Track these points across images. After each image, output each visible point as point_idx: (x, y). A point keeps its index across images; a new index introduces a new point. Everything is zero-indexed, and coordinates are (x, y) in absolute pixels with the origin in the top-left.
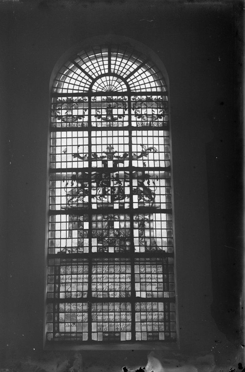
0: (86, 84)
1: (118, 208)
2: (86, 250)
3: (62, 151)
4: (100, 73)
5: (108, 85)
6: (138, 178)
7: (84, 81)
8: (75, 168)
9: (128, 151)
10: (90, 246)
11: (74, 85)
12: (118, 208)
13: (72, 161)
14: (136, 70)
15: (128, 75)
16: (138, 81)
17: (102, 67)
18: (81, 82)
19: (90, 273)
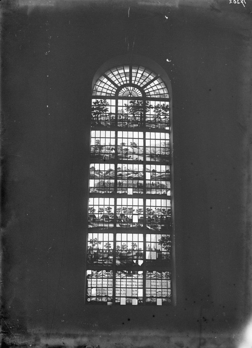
0: (112, 91)
1: (137, 304)
2: (117, 213)
3: (124, 104)
4: (136, 83)
5: (126, 91)
6: (160, 122)
7: (110, 88)
8: (113, 131)
9: (142, 296)
10: (118, 223)
11: (108, 89)
12: (137, 304)
13: (100, 138)
14: (152, 81)
15: (144, 84)
16: (152, 87)
17: (141, 81)
18: (108, 89)
19: (114, 279)
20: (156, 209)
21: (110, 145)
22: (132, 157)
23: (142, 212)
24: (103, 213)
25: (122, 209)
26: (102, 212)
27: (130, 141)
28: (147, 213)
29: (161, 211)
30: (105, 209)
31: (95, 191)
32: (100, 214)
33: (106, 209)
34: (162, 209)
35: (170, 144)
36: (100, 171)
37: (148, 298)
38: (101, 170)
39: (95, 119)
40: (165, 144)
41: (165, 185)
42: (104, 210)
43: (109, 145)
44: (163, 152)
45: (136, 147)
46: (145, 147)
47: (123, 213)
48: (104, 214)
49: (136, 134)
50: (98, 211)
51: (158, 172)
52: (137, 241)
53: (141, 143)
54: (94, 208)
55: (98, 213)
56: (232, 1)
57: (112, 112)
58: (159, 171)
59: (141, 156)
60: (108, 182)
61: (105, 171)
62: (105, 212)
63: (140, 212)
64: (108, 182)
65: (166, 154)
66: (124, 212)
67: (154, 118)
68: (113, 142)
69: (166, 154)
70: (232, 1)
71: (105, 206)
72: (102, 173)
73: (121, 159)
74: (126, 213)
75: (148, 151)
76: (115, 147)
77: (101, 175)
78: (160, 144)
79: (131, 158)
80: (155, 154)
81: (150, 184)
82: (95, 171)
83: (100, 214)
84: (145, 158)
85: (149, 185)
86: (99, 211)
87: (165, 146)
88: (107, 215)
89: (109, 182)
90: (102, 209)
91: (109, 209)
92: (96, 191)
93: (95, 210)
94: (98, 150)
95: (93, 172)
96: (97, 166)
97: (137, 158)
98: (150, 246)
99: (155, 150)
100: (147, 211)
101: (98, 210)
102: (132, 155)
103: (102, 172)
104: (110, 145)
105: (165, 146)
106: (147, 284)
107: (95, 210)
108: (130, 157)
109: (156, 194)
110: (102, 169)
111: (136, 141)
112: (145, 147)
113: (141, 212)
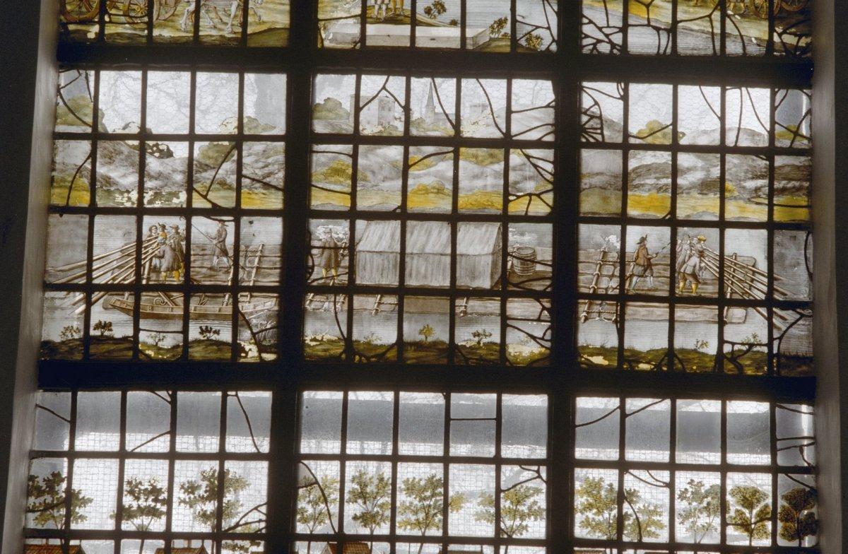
20: (671, 485)
23: (529, 522)
24: (158, 525)
25: (349, 486)
26: (153, 512)
28: (587, 523)
29: (724, 508)
30: (178, 494)
31: (94, 321)
32: (130, 535)
33: (191, 488)
34: (729, 488)
36: (144, 135)
37: (502, 525)
38: (154, 126)
41: (763, 266)
42: (169, 502)
47: (352, 528)
48: (168, 535)
50: (111, 506)
54: (75, 486)
55: (110, 525)
56: (611, 552)
58: (703, 141)
59: (538, 343)
60: (221, 237)
62: (184, 519)
63: (514, 514)
64: (221, 237)
66: (366, 518)
70: (611, 552)
71: (179, 464)
72: (169, 154)
74: (377, 532)
77: (159, 176)
79: (446, 17)
81: (614, 256)
82: (97, 136)
83: (130, 535)
85: (608, 270)
86: (122, 513)
88: (196, 544)
89: (230, 240)
90: (155, 491)
91: (219, 486)
92: (107, 326)
93: (85, 502)
95: (86, 146)
96: (119, 96)
97: (501, 23)
100: (589, 507)
101: (114, 494)
103: (163, 145)
107: (85, 502)
109: (671, 353)
113: (523, 517)
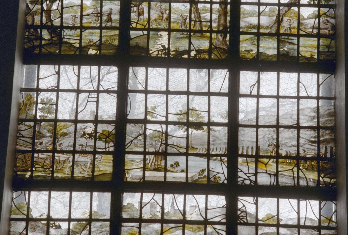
21: (96, 121)
22: (183, 166)
27: (178, 104)
35: (333, 114)
36: (49, 219)
38: (53, 215)
39: (37, 19)
40: (315, 114)
43: (92, 118)
44: (307, 146)
45: (198, 126)
46: (233, 125)
49: (198, 77)
51: (286, 226)
52: (185, 89)
53: (220, 108)
57: (215, 119)
61: (69, 220)
65: (323, 151)
67: (275, 18)
68: (108, 108)
69: (323, 151)
72: (59, 227)
73: (229, 6)
75: (247, 138)
76: (116, 128)
78: (296, 113)
80: (277, 152)
84: (233, 168)
87: (318, 122)
94: (44, 140)
95: (24, 224)
98: (179, 35)
99: (275, 137)
102: (184, 158)
103: (57, 223)
104: (96, 121)
105: (316, 120)
106: (185, 80)
108: (177, 164)
110: (59, 210)
111: (199, 103)
112: (233, 125)
